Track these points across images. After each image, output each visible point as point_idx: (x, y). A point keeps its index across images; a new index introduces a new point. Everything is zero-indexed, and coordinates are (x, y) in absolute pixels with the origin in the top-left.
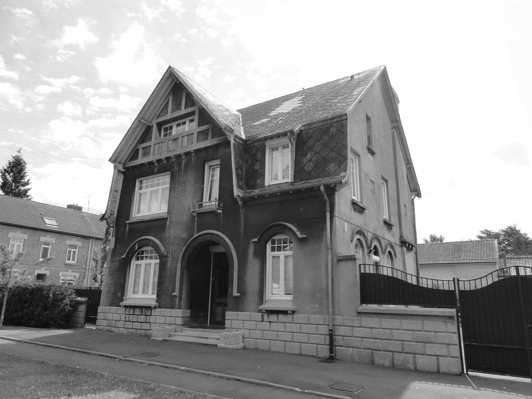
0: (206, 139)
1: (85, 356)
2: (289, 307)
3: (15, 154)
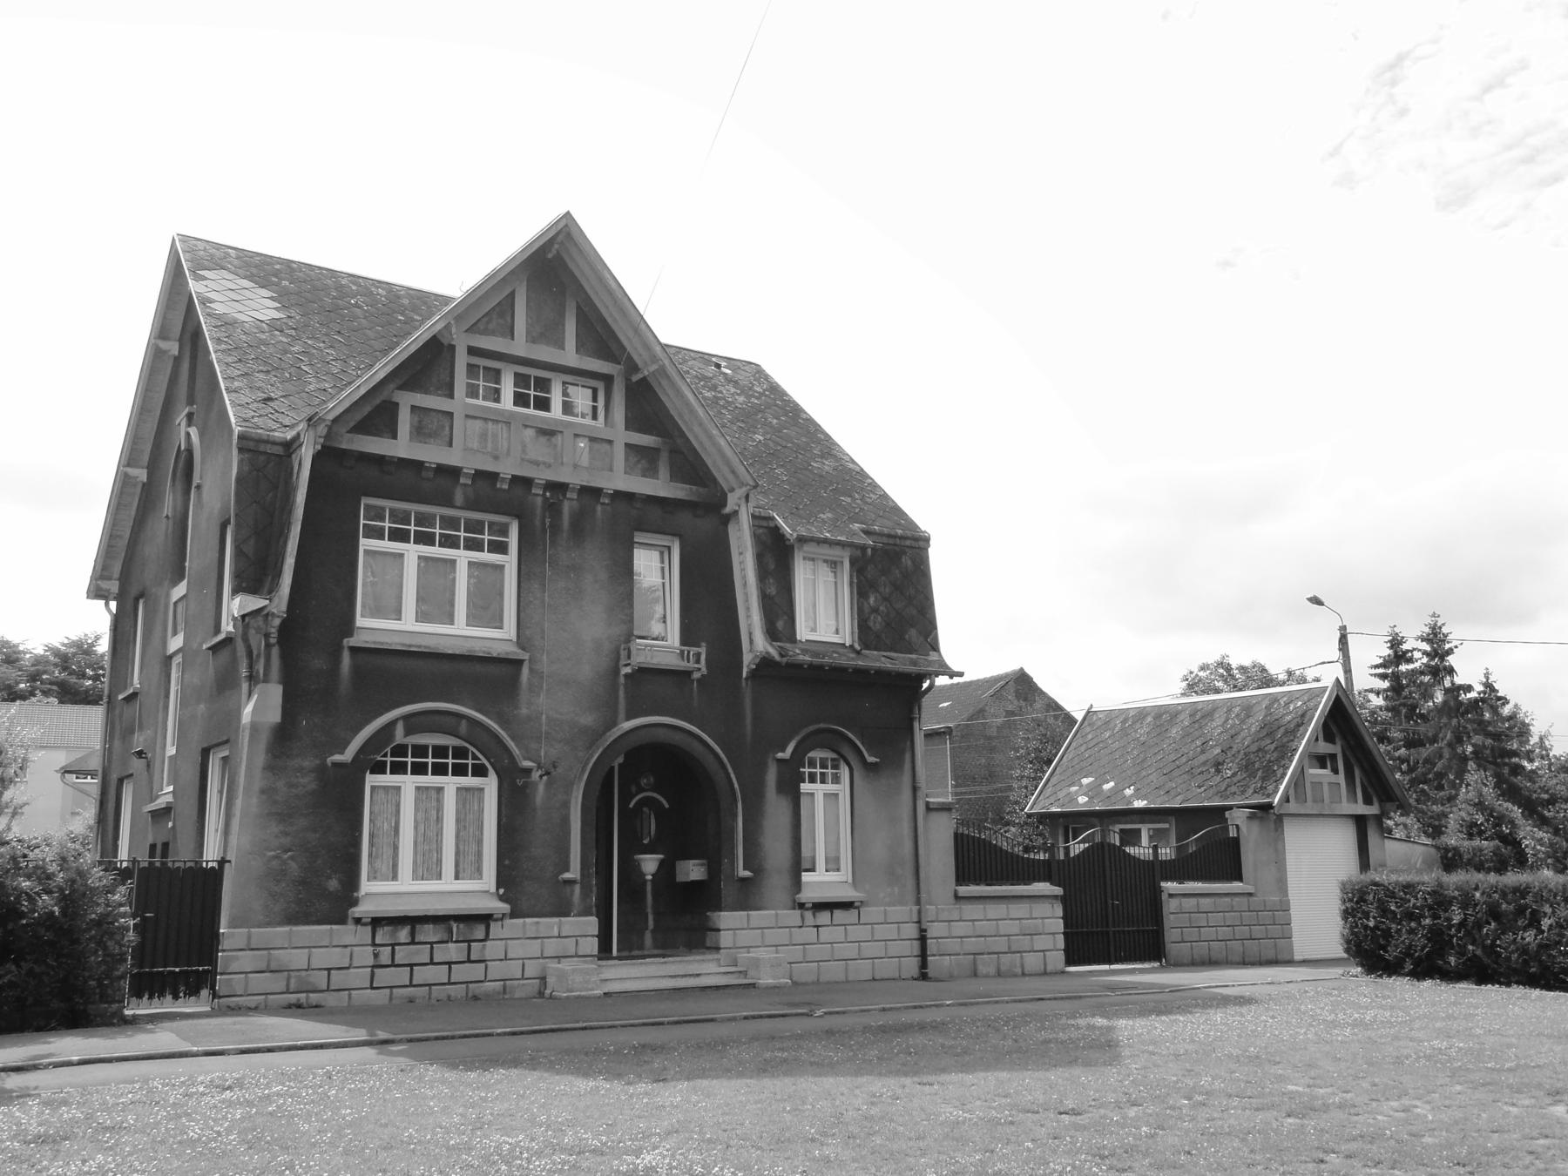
0: (651, 471)
1: (709, 1025)
2: (848, 894)
3: (1429, 620)
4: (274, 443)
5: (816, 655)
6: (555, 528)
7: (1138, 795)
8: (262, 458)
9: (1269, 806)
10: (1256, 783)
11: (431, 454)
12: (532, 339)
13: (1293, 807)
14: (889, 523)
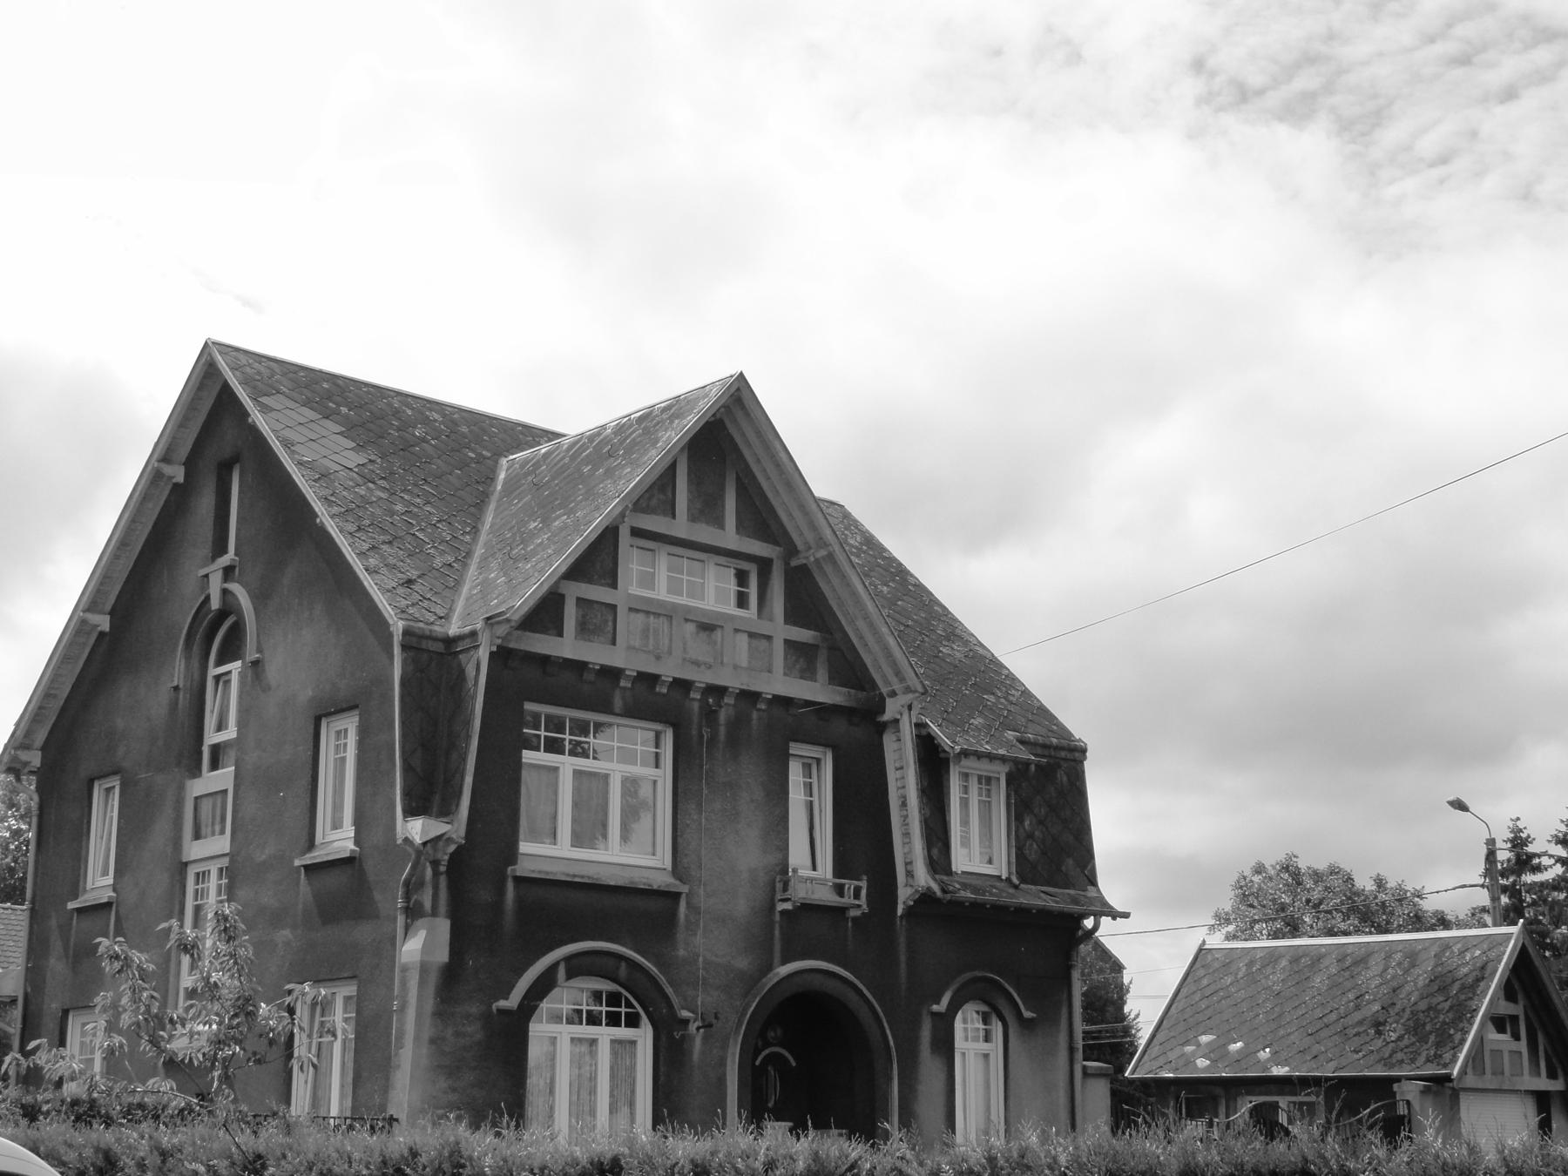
0: (808, 673)
4: (435, 639)
5: (975, 890)
6: (713, 740)
7: (1276, 1059)
8: (425, 656)
9: (1448, 1078)
10: (1428, 1050)
11: (596, 654)
12: (693, 518)
13: (1471, 1081)
14: (1043, 731)
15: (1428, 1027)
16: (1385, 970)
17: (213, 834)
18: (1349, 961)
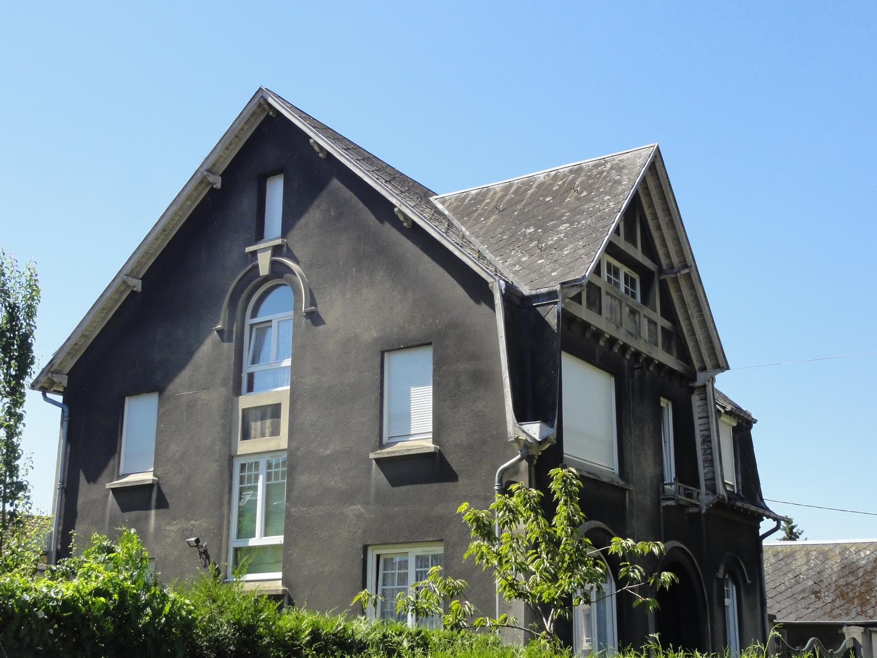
15: (851, 595)
16: (808, 561)
17: (263, 435)
18: (781, 556)
